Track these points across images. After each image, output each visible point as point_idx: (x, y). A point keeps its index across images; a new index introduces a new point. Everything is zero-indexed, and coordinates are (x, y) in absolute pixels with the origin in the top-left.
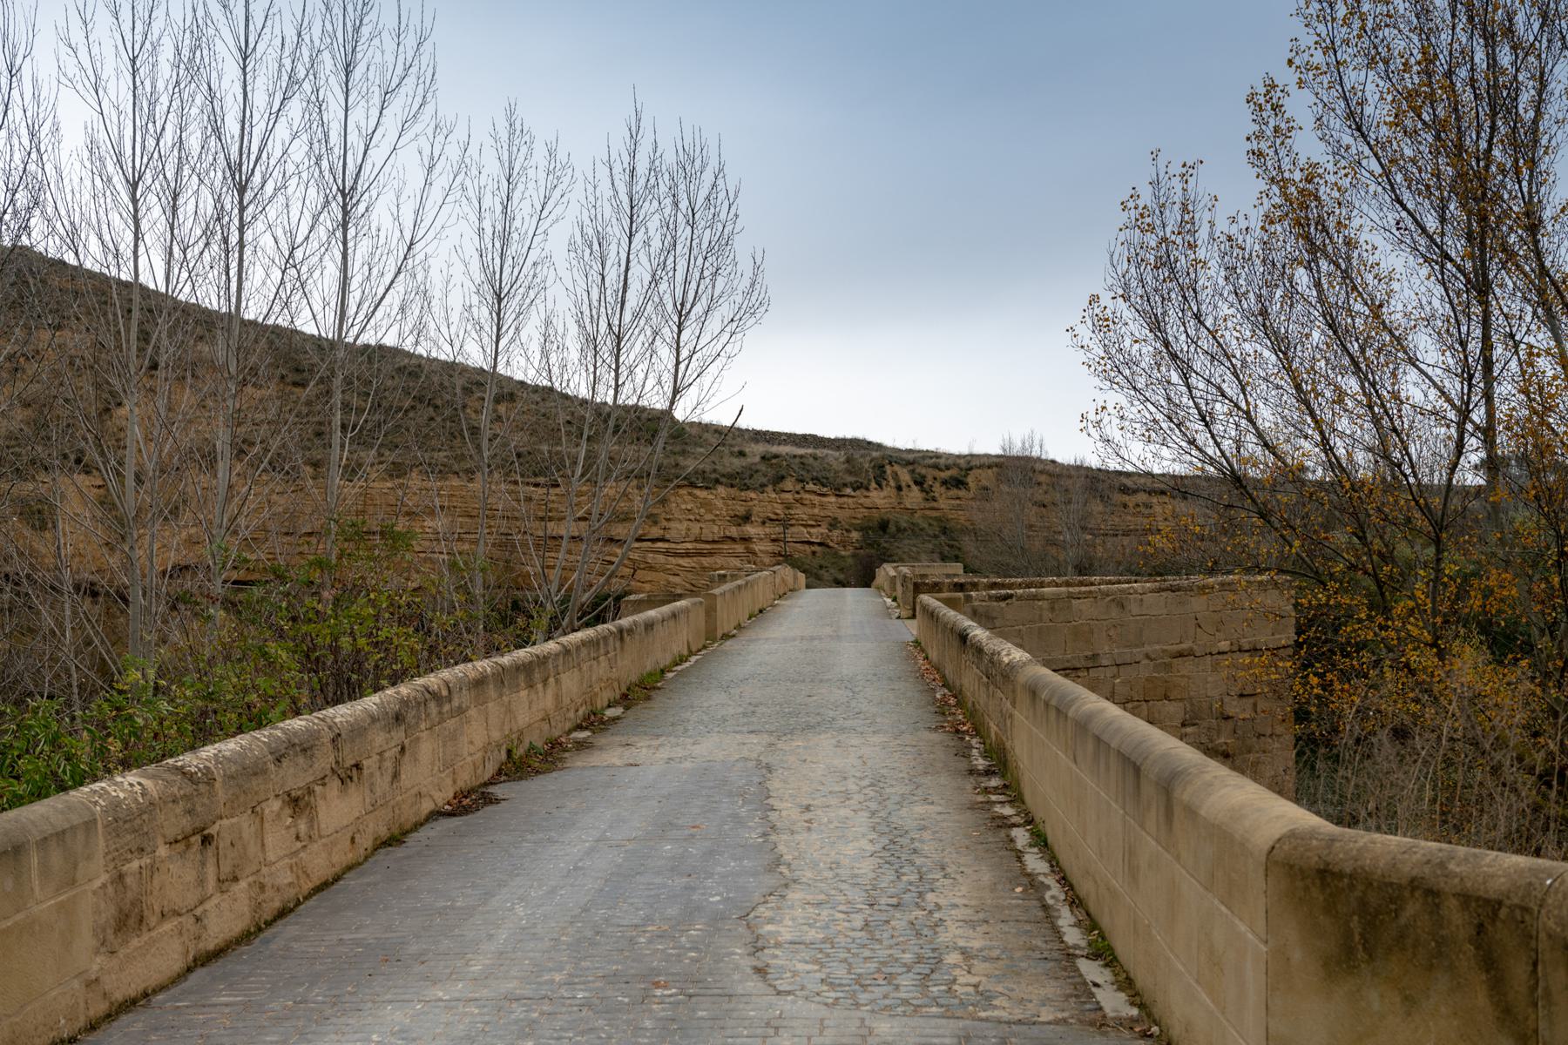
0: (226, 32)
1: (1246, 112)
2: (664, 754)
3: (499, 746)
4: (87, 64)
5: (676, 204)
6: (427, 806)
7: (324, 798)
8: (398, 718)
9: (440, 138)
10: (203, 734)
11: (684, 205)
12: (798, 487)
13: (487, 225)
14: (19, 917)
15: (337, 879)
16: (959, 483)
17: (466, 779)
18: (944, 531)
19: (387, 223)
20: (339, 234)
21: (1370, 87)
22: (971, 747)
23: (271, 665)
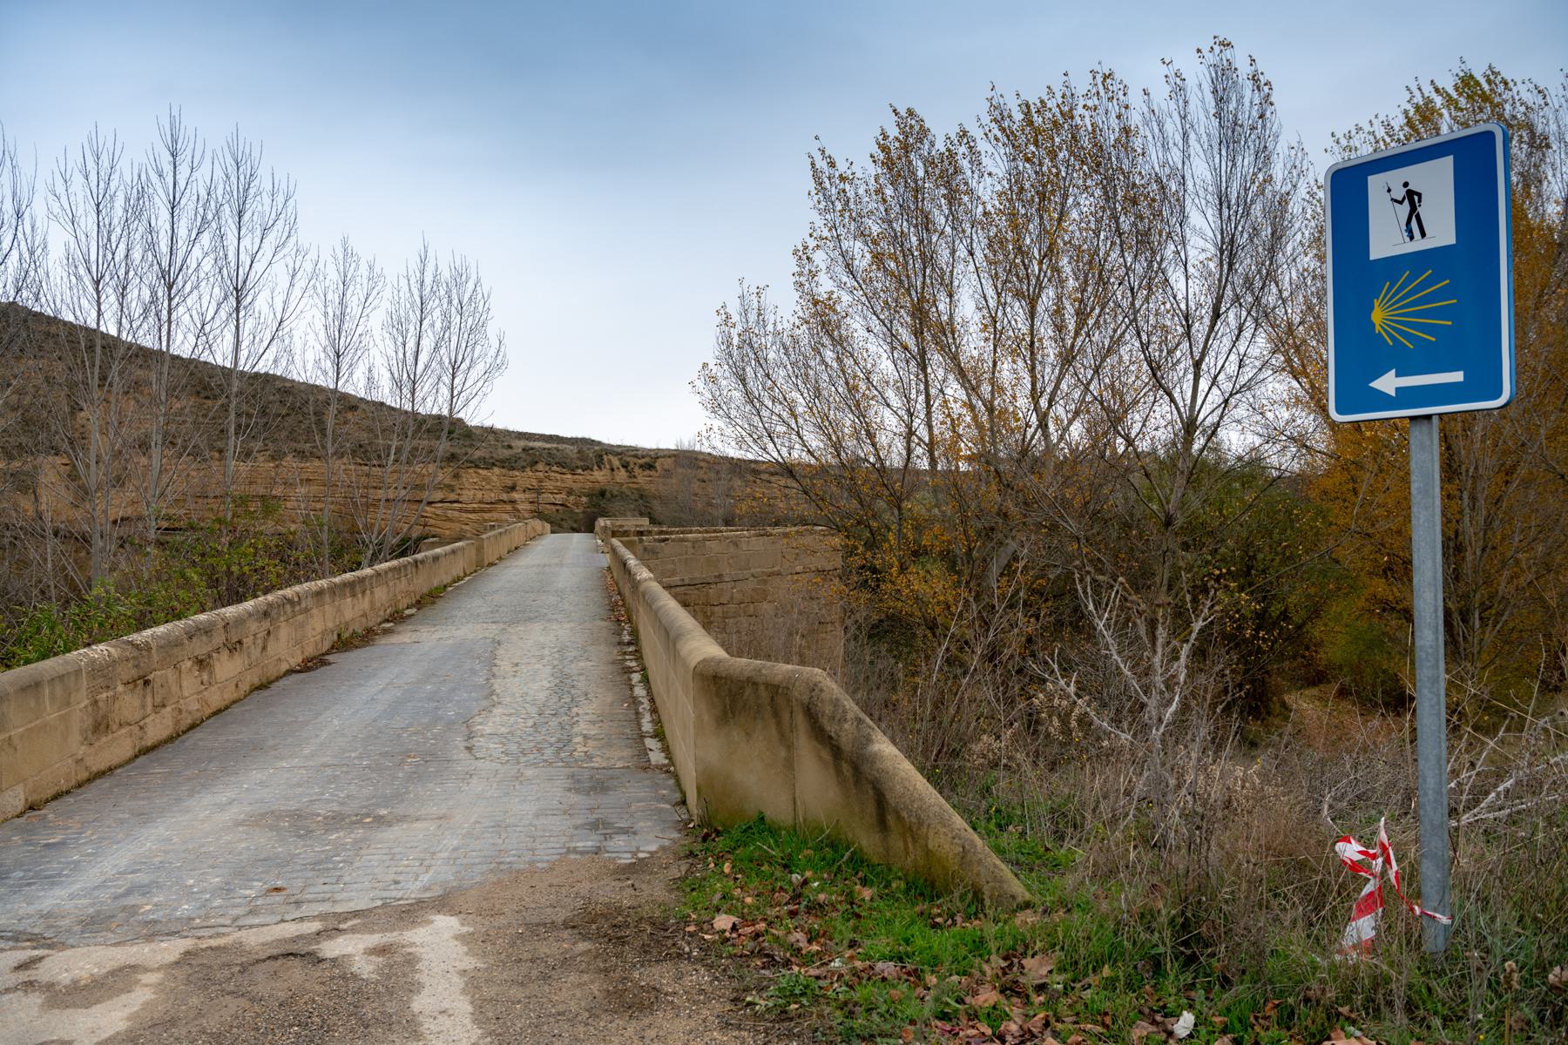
0: (161, 192)
1: (793, 261)
2: (437, 636)
3: (332, 632)
4: (67, 206)
5: (450, 302)
6: (284, 667)
7: (219, 660)
8: (266, 614)
9: (300, 258)
10: (141, 625)
11: (455, 302)
12: (547, 468)
13: (330, 310)
14: (38, 722)
15: (227, 708)
16: (650, 467)
17: (310, 651)
18: (641, 496)
19: (265, 309)
20: (234, 315)
21: (856, 250)
22: (623, 629)
23: (187, 583)
